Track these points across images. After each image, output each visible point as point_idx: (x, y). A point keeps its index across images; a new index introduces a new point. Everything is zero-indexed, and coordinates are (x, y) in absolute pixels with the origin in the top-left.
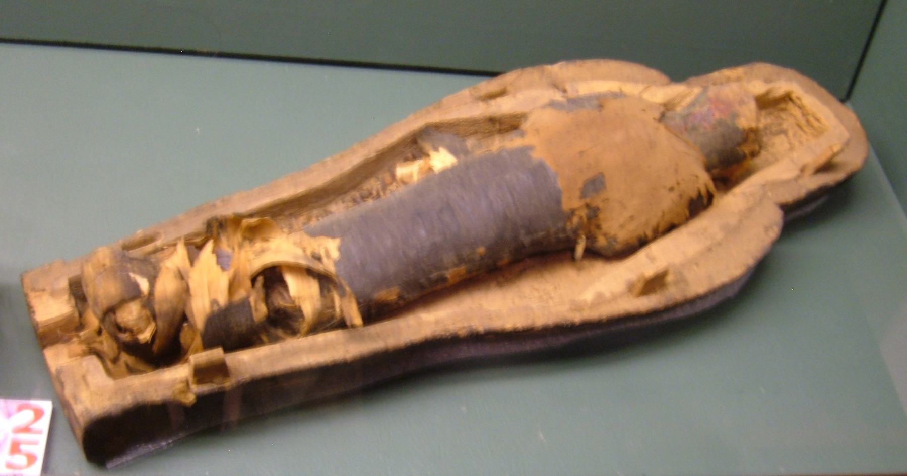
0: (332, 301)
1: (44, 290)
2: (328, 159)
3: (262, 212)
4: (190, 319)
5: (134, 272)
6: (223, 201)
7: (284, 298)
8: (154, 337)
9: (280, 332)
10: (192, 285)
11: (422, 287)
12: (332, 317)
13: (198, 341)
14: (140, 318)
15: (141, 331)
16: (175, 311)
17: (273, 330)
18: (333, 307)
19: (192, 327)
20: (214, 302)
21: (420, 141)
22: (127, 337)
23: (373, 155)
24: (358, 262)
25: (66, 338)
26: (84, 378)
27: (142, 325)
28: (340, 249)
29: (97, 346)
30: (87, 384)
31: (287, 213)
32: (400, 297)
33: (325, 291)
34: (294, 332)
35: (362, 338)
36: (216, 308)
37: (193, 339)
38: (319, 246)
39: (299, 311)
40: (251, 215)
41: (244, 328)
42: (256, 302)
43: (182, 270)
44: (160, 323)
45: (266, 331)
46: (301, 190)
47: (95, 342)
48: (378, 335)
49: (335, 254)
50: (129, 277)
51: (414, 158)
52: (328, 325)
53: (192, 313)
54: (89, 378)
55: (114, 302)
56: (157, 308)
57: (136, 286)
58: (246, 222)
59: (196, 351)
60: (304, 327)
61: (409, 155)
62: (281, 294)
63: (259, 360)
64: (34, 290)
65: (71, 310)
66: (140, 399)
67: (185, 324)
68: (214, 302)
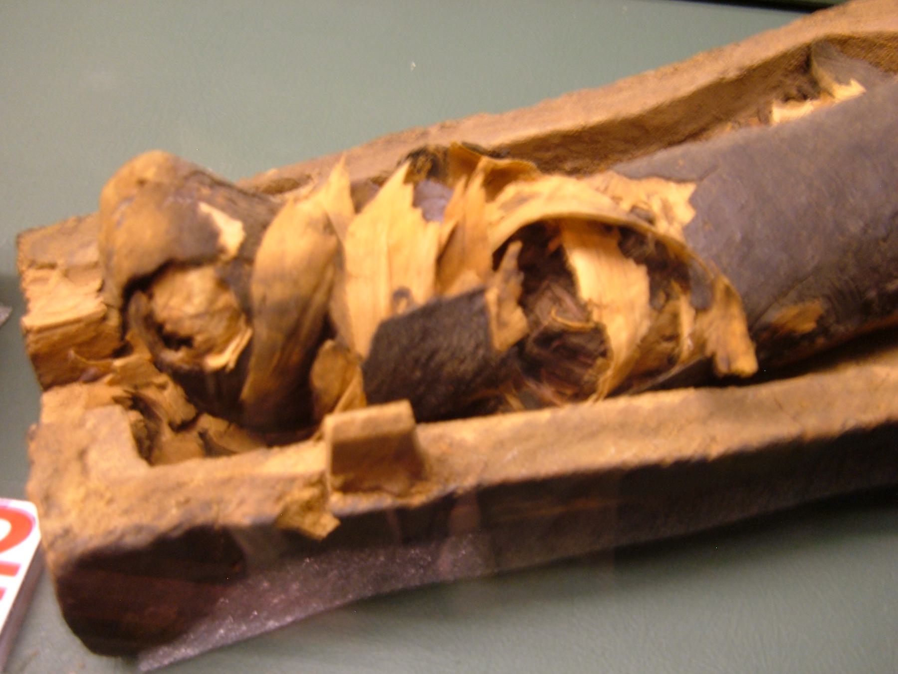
0: (675, 317)
1: (52, 266)
2: (651, 73)
3: (517, 150)
4: (342, 331)
5: (210, 202)
6: (443, 127)
7: (564, 312)
8: (244, 356)
9: (547, 392)
10: (350, 248)
11: (866, 308)
12: (671, 360)
13: (355, 386)
14: (209, 313)
15: (212, 348)
16: (304, 306)
17: (531, 385)
18: (674, 337)
19: (343, 349)
20: (400, 294)
21: (815, 64)
22: (182, 360)
23: (732, 74)
24: (738, 237)
25: (92, 371)
26: (82, 454)
27: (217, 328)
28: (693, 201)
29: (150, 393)
30: (85, 470)
31: (568, 166)
32: (822, 328)
33: (662, 296)
34: (581, 393)
35: (741, 412)
36: (402, 308)
37: (345, 383)
38: (649, 196)
39: (598, 332)
40: (495, 154)
41: (469, 366)
42: (500, 302)
43: (332, 217)
44: (263, 329)
45: (518, 386)
46: (597, 118)
47: (148, 385)
48: (779, 407)
49: (685, 214)
50: (194, 208)
51: (804, 97)
52: (662, 378)
53: (345, 316)
54: (93, 456)
55: (149, 265)
56: (257, 291)
57: (212, 234)
58: (484, 162)
59: (348, 407)
60: (607, 378)
61: (794, 92)
62: (557, 301)
63: (501, 445)
64: (32, 264)
65: (99, 309)
66: (202, 518)
67: (329, 344)
68: (400, 294)
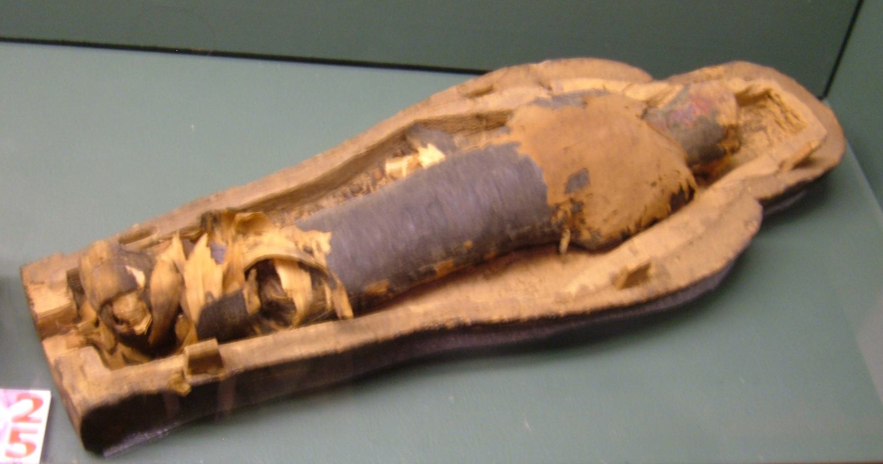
0: (324, 293)
1: (43, 283)
2: (319, 155)
3: (255, 207)
4: (185, 311)
5: (130, 265)
6: (217, 196)
7: (276, 291)
8: (149, 329)
9: (272, 324)
10: (187, 278)
11: (411, 280)
12: (324, 309)
13: (193, 332)
14: (136, 310)
15: (137, 323)
16: (170, 303)
17: (265, 322)
18: (324, 300)
19: (187, 319)
20: (208, 294)
21: (408, 138)
22: (124, 328)
23: (363, 151)
24: (349, 255)
25: (64, 329)
26: (82, 368)
27: (138, 316)
28: (331, 243)
29: (94, 337)
30: (85, 375)
31: (279, 208)
32: (390, 290)
33: (317, 284)
34: (286, 324)
35: (352, 330)
36: (210, 300)
37: (188, 331)
38: (311, 240)
39: (292, 303)
40: (244, 210)
41: (237, 320)
42: (249, 294)
43: (177, 263)
44: (156, 315)
45: (259, 323)
46: (293, 185)
47: (93, 333)
48: (368, 327)
49: (326, 248)
50: (125, 270)
51: (403, 154)
52: (319, 317)
53: (187, 305)
54: (87, 369)
55: (111, 294)
56: (153, 300)
57: (132, 279)
58: (239, 217)
59: (191, 343)
60: (296, 318)
61: (399, 151)
62: (274, 287)
63: (252, 351)
64: (33, 282)
65: (69, 302)
66: (136, 389)
67: (180, 316)
68: (208, 294)
